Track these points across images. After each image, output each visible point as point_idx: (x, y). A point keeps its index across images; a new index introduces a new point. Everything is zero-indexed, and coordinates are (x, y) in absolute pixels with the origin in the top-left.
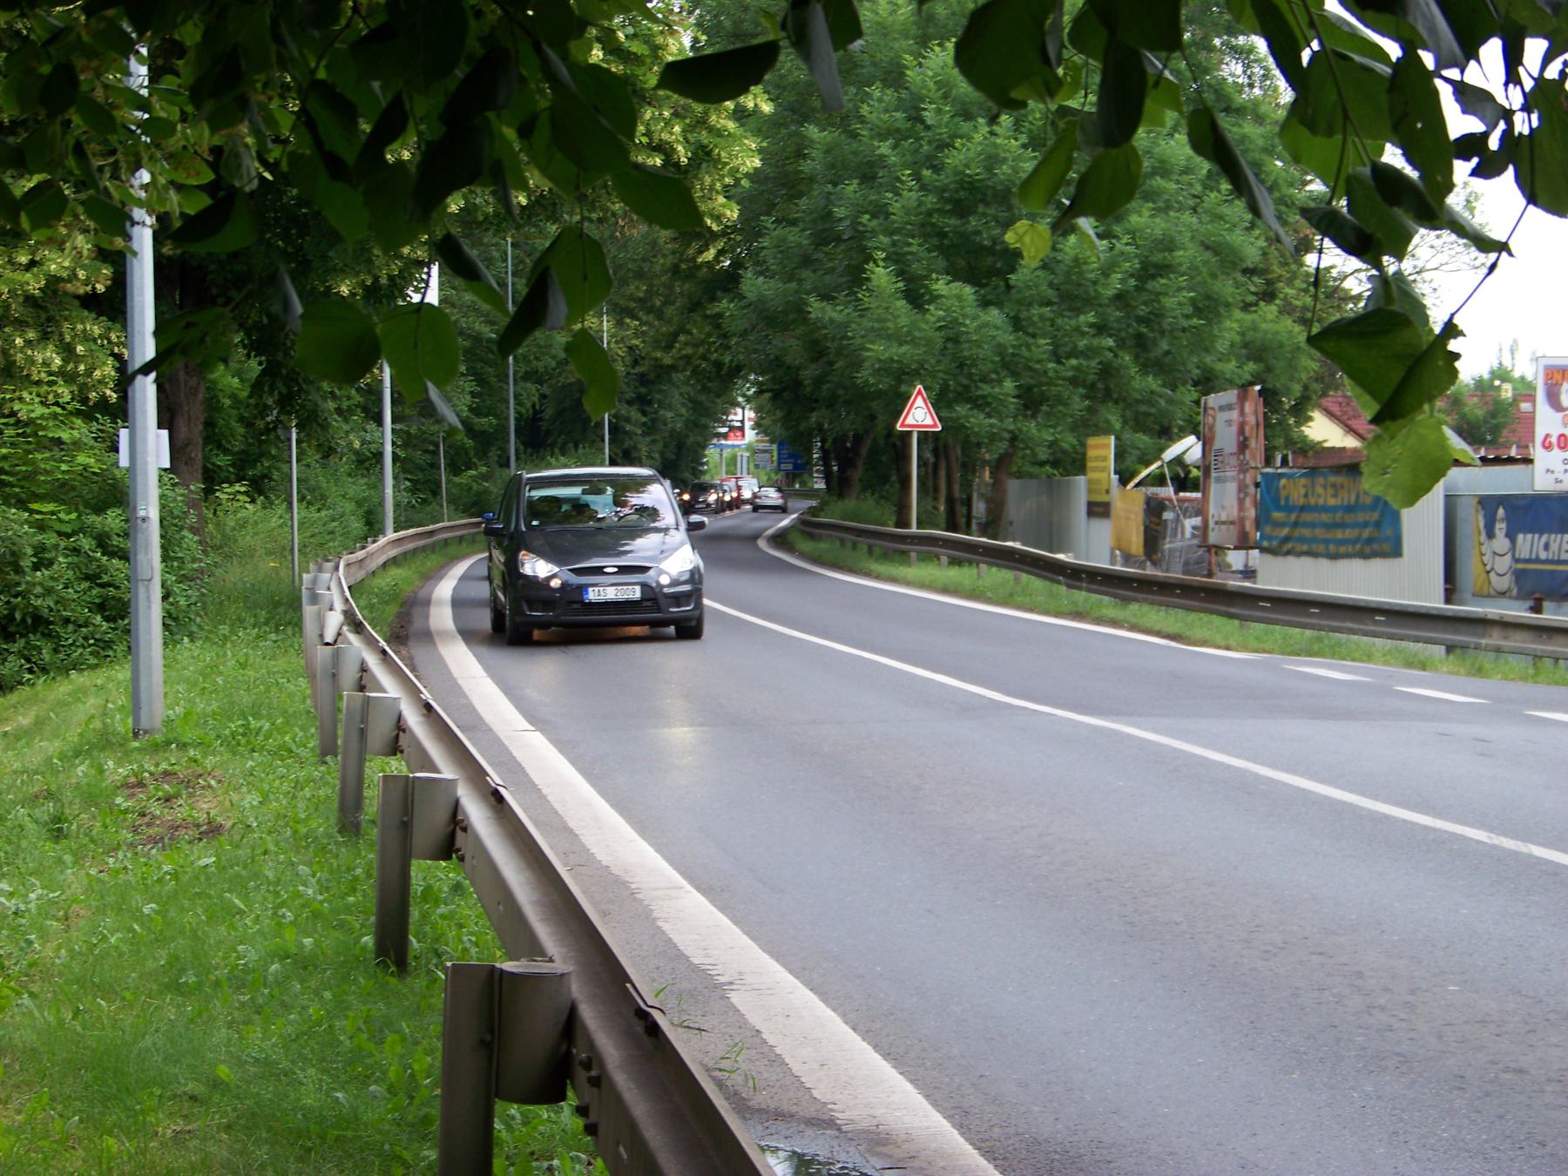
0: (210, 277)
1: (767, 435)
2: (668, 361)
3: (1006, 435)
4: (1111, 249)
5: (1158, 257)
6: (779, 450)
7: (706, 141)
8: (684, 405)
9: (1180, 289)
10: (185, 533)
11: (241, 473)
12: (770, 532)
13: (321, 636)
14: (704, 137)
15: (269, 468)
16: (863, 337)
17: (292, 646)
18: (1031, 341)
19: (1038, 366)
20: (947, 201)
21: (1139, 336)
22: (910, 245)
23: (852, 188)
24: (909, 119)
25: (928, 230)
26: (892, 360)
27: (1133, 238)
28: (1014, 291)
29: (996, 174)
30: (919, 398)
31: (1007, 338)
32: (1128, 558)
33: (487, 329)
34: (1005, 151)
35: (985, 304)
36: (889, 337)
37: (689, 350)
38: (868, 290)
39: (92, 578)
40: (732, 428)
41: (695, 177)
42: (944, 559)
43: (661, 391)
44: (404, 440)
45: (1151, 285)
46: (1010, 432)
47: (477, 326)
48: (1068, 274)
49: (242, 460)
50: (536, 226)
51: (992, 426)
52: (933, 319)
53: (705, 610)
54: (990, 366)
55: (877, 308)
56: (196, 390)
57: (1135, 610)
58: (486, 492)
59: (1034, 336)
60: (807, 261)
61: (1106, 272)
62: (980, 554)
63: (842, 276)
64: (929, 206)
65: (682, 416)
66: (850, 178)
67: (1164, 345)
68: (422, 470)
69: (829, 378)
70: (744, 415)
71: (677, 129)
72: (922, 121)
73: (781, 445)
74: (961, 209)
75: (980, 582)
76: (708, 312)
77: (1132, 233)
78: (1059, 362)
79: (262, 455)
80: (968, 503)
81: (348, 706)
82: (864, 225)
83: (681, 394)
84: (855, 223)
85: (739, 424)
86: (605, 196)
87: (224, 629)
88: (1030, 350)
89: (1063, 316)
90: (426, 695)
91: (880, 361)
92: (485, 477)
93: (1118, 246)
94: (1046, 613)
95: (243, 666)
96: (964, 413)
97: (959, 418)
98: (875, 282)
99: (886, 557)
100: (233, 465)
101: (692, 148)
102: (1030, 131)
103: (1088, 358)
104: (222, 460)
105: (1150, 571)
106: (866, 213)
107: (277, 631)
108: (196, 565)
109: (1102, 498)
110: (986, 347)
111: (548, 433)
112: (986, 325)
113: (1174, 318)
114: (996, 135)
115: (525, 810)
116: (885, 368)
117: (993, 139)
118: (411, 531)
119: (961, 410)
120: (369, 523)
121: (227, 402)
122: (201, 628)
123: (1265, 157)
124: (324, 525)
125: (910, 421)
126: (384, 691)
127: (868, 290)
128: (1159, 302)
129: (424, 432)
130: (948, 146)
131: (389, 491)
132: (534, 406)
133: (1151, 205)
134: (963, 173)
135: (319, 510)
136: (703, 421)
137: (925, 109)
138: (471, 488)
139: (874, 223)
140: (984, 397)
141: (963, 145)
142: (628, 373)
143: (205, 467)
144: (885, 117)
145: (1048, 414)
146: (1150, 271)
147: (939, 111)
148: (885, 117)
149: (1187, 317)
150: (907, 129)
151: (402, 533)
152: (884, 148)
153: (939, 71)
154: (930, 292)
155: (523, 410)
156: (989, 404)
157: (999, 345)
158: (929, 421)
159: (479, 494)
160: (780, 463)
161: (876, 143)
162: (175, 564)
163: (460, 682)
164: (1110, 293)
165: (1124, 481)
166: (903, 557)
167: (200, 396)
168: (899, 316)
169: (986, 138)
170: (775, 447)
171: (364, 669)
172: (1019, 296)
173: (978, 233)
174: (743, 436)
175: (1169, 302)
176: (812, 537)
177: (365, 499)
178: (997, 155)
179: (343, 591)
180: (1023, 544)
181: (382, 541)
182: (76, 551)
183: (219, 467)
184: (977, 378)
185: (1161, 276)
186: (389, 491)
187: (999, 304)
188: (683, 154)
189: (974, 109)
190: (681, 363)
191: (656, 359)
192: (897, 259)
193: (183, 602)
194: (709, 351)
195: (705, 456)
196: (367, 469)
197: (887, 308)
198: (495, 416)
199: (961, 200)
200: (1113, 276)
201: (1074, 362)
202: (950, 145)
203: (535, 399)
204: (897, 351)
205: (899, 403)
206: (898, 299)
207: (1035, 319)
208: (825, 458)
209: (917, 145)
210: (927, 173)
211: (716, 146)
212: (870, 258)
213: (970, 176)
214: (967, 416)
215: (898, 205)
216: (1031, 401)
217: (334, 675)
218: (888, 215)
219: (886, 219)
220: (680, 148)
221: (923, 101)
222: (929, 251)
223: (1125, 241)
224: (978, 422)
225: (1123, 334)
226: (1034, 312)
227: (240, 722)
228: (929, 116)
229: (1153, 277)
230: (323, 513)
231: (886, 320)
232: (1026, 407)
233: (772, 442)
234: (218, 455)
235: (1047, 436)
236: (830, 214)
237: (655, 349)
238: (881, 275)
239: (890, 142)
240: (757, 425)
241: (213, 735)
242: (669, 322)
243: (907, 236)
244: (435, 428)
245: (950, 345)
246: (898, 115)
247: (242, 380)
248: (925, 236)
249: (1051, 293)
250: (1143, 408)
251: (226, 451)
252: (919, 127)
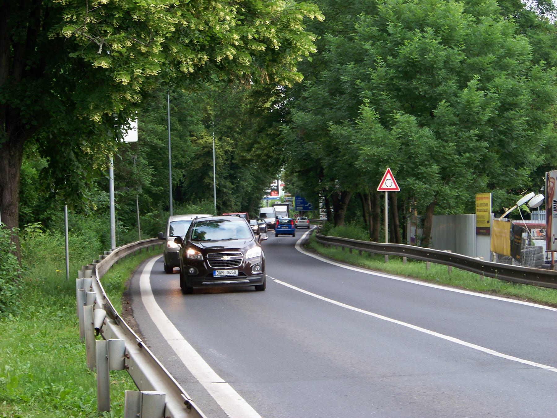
0: (21, 114)
1: (290, 193)
2: (249, 157)
3: (434, 193)
4: (486, 95)
5: (510, 99)
6: (296, 200)
7: (288, 37)
8: (252, 179)
9: (521, 116)
10: (10, 255)
11: (37, 217)
12: (299, 242)
13: (93, 324)
14: (288, 35)
15: (50, 214)
16: (358, 143)
17: (70, 320)
18: (446, 144)
19: (449, 157)
20: (400, 72)
21: (501, 141)
22: (381, 95)
23: (351, 66)
24: (379, 30)
25: (391, 87)
26: (374, 155)
27: (497, 90)
28: (435, 118)
29: (426, 58)
30: (389, 174)
31: (433, 143)
32: (500, 257)
33: (160, 142)
34: (430, 46)
35: (421, 125)
36: (372, 143)
37: (259, 152)
38: (361, 119)
40: (272, 190)
41: (282, 56)
42: (405, 258)
43: (240, 172)
44: (120, 200)
45: (506, 114)
46: (435, 191)
47: (155, 141)
48: (464, 109)
49: (37, 210)
50: (198, 84)
51: (426, 188)
52: (395, 133)
53: (267, 280)
54: (425, 157)
55: (366, 128)
56: (14, 176)
57: (526, 289)
58: (158, 223)
59: (447, 141)
62: (428, 257)
63: (345, 112)
64: (391, 75)
65: (251, 184)
66: (350, 61)
67: (513, 145)
68: (127, 213)
69: (336, 165)
70: (279, 184)
71: (273, 31)
72: (386, 31)
73: (297, 198)
74: (408, 76)
75: (428, 272)
76: (269, 133)
77: (497, 87)
78: (460, 155)
79: (47, 208)
80: (404, 229)
81: (128, 401)
82: (358, 85)
83: (251, 174)
84: (353, 84)
85: (276, 188)
86: (235, 67)
87: (32, 308)
88: (445, 149)
89: (462, 131)
90: (187, 396)
91: (368, 155)
92: (156, 216)
93: (489, 94)
94: (474, 290)
95: (44, 335)
96: (411, 182)
97: (409, 185)
98: (364, 114)
99: (369, 256)
100: (33, 213)
101: (281, 41)
102: (443, 36)
103: (475, 153)
104: (27, 210)
105: (514, 265)
106: (358, 79)
107: (61, 309)
108: (15, 273)
109: (486, 225)
110: (423, 147)
111: (185, 194)
112: (423, 136)
113: (518, 131)
114: (425, 38)
115: (158, 359)
116: (371, 159)
117: (423, 40)
118: (125, 246)
119: (411, 180)
120: (103, 242)
121: (30, 181)
122: (19, 308)
123: (551, 50)
124: (80, 244)
125: (384, 186)
126: (153, 389)
127: (361, 119)
128: (511, 123)
129: (129, 195)
130: (400, 44)
131: (113, 225)
132: (180, 180)
133: (505, 72)
134: (409, 58)
135: (78, 236)
136: (261, 187)
137: (388, 25)
138: (150, 222)
139: (363, 84)
140: (422, 173)
141: (408, 43)
142: (225, 164)
143: (20, 216)
144: (367, 29)
145: (455, 182)
146: (505, 107)
147: (395, 26)
148: (367, 29)
149: (524, 130)
150: (379, 36)
151: (121, 248)
152: (367, 45)
153: (395, 5)
154: (393, 119)
155: (176, 182)
156: (425, 177)
157: (429, 146)
158: (394, 186)
159: (154, 225)
160: (296, 206)
161: (363, 43)
162: (4, 273)
163: (169, 343)
164: (486, 118)
166: (381, 257)
167: (17, 179)
168: (377, 132)
169: (420, 39)
170: (294, 198)
171: (126, 355)
172: (438, 121)
173: (417, 88)
174: (278, 193)
175: (516, 123)
176: (324, 245)
177: (100, 230)
178: (426, 48)
179: (101, 292)
180: (452, 252)
181: (112, 253)
183: (26, 214)
184: (418, 164)
185: (512, 110)
186: (113, 225)
187: (428, 125)
188: (276, 44)
189: (413, 25)
190: (255, 158)
191: (243, 156)
192: (374, 102)
193: (8, 294)
194: (269, 152)
195: (261, 204)
196: (101, 214)
197: (371, 128)
198: (162, 186)
199: (407, 72)
200: (487, 109)
201: (468, 155)
202: (401, 43)
203: (181, 176)
204: (377, 150)
205: (377, 177)
206: (376, 123)
207: (447, 132)
208: (327, 205)
209: (384, 43)
210: (390, 58)
211: (294, 39)
212: (361, 102)
213: (413, 59)
214: (413, 184)
215: (375, 75)
217: (107, 358)
218: (370, 80)
219: (369, 82)
220: (275, 41)
221: (387, 21)
222: (392, 98)
223: (492, 91)
224: (419, 186)
225: (492, 140)
226: (446, 128)
227: (46, 387)
228: (390, 29)
229: (507, 110)
230: (80, 238)
231: (370, 134)
232: (443, 178)
233: (292, 196)
234: (25, 208)
235: (454, 193)
236: (338, 80)
237: (242, 151)
239: (370, 42)
240: (285, 188)
241: (29, 394)
242: (249, 138)
243: (380, 90)
244: (134, 192)
245: (404, 147)
246: (374, 28)
247: (37, 170)
248: (390, 90)
249: (455, 119)
250: (502, 178)
251: (29, 206)
252: (385, 34)
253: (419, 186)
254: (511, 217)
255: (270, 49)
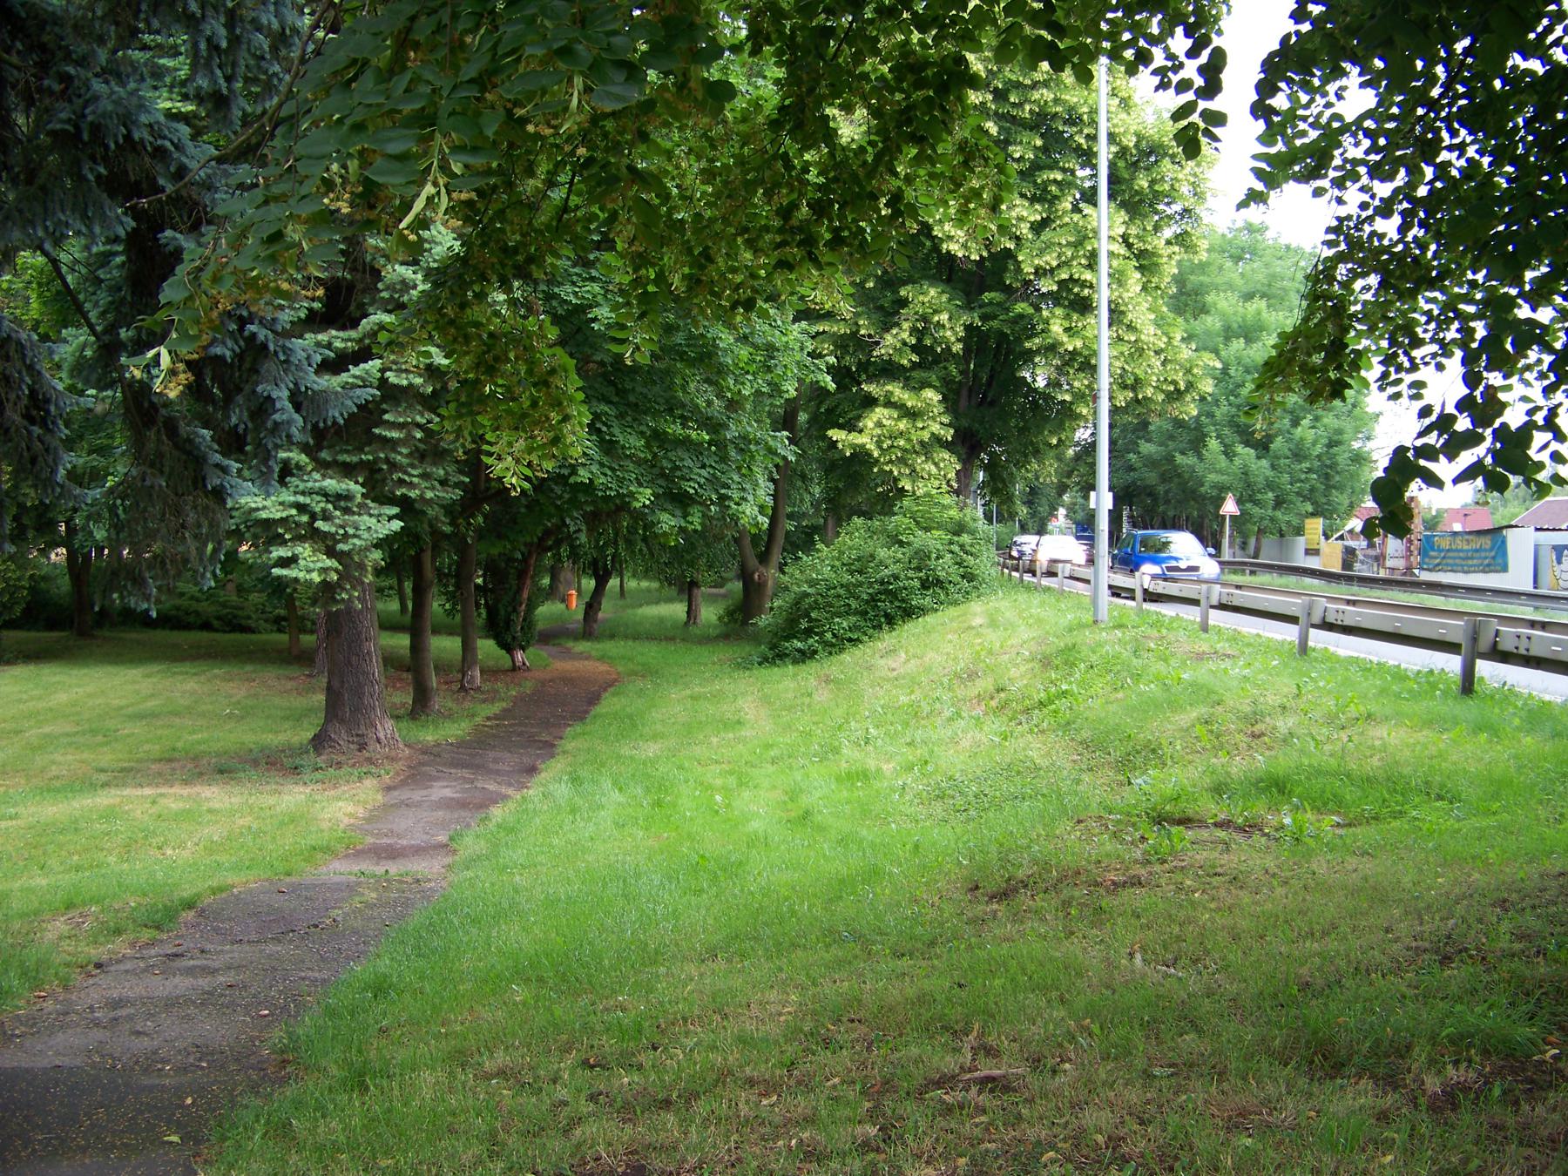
25: (1233, 423)
31: (1269, 473)
35: (1259, 458)
39: (959, 564)
60: (1172, 437)
61: (1314, 443)
105: (1408, 578)
119: (1248, 505)
165: (1327, 537)
175: (1340, 459)
182: (951, 552)
205: (1219, 501)
216: (1279, 503)
228: (1232, 372)
238: (1213, 444)
253: (1256, 511)
254: (1341, 538)
255: (1177, 390)
